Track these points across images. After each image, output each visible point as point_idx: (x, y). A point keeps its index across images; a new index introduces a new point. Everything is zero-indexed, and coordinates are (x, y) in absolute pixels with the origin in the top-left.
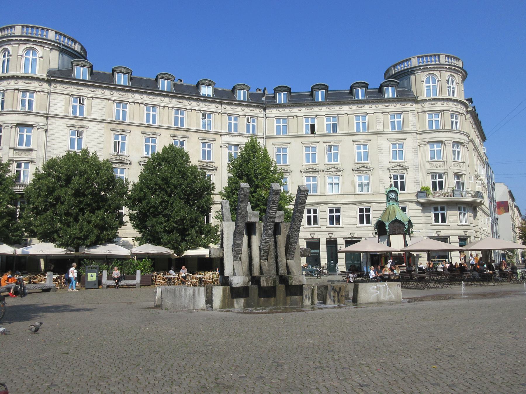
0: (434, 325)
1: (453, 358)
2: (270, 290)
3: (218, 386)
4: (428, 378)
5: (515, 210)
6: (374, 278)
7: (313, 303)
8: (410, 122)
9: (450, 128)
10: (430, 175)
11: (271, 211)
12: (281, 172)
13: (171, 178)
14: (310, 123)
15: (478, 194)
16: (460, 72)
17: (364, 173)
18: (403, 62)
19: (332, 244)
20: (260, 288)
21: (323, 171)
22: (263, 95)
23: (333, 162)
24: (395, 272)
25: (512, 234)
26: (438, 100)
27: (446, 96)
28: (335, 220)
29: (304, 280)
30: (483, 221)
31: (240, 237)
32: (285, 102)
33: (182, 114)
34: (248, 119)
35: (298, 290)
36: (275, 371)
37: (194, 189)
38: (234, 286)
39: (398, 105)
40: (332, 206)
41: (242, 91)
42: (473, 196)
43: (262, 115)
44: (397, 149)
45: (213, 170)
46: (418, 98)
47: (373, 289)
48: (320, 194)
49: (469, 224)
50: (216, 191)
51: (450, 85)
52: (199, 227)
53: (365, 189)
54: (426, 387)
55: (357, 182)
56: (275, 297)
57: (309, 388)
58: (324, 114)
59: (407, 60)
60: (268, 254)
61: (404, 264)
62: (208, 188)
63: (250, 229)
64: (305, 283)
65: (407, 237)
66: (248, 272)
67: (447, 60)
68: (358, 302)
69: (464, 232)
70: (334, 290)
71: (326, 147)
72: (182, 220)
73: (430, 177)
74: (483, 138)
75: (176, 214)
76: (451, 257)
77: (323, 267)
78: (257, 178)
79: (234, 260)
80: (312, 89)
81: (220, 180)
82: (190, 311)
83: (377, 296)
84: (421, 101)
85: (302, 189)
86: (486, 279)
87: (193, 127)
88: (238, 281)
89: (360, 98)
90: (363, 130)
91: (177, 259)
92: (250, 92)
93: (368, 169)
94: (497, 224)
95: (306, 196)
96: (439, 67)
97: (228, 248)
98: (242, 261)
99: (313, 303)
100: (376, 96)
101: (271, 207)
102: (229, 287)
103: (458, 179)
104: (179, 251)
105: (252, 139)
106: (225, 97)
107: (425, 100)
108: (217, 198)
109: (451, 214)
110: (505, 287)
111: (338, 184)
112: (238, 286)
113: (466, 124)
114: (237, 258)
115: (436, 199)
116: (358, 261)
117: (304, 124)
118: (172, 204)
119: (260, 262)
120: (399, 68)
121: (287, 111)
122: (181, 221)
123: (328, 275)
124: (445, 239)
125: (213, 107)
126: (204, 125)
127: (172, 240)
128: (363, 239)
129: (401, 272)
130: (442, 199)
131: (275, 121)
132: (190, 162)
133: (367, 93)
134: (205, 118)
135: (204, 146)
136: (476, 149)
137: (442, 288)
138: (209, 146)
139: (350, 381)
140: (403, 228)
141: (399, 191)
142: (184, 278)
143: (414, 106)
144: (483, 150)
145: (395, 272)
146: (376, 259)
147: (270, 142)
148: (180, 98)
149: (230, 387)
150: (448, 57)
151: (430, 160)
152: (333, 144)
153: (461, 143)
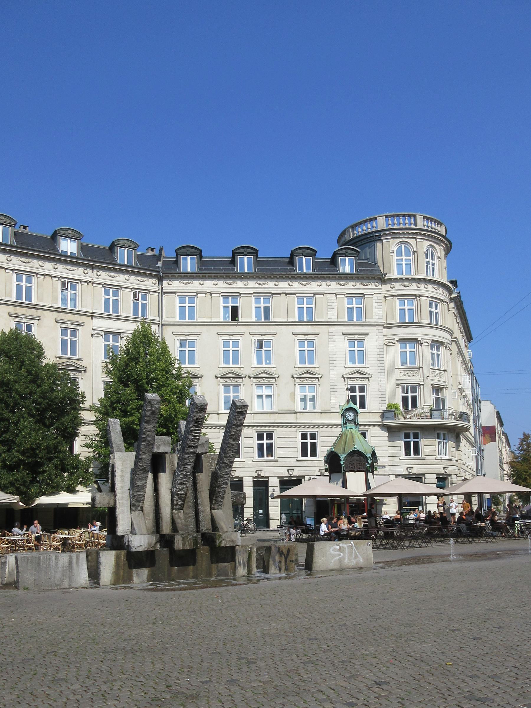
0: (434, 598)
1: (480, 641)
2: (187, 555)
3: (177, 697)
4: (460, 669)
5: (503, 438)
6: (326, 534)
7: (249, 573)
8: (374, 310)
9: (428, 321)
10: (400, 387)
11: (191, 437)
12: (188, 377)
13: (16, 382)
14: (230, 305)
15: (462, 416)
16: (442, 241)
17: (309, 382)
18: (366, 221)
19: (261, 485)
20: (173, 552)
21: (249, 377)
22: (159, 258)
23: (264, 365)
24: (357, 525)
25: (499, 472)
26: (413, 279)
27: (422, 275)
28: (266, 450)
29: (238, 538)
30: (467, 453)
31: (143, 475)
32: (193, 271)
33: (29, 281)
34: (135, 295)
35: (229, 554)
36: (248, 670)
37: (52, 401)
38: (134, 550)
39: (358, 284)
40: (261, 430)
41: (126, 251)
42: (455, 419)
43: (156, 289)
44: (356, 349)
45: (80, 371)
46: (385, 275)
47: (335, 550)
48: (319, 411)
49: (451, 458)
50: (87, 404)
51: (430, 260)
52: (62, 460)
53: (309, 404)
54: (463, 681)
55: (299, 394)
56: (194, 565)
57: (309, 690)
58: (252, 292)
59: (371, 220)
60: (184, 501)
61: (365, 514)
62: (74, 400)
63: (157, 463)
64: (239, 544)
65: (370, 475)
66: (153, 529)
67: (426, 223)
68: (313, 569)
69: (444, 468)
70: (281, 553)
71: (253, 341)
72: (33, 450)
73: (400, 389)
74: (469, 338)
75: (24, 439)
76: (426, 504)
77: (248, 519)
78: (151, 385)
79: (132, 510)
80: (235, 253)
81: (93, 386)
82: (65, 591)
83: (340, 560)
84: (390, 280)
85: (238, 404)
86: (475, 533)
87: (47, 302)
88: (140, 542)
89: (305, 271)
90: (308, 318)
91: (23, 511)
92: (138, 252)
93: (315, 376)
94: (482, 457)
95: (244, 414)
96: (416, 233)
97: (123, 493)
98: (145, 512)
99: (249, 573)
100: (327, 269)
101: (192, 431)
102: (125, 551)
103: (437, 394)
104: (27, 498)
105: (143, 325)
106: (97, 257)
107: (396, 280)
108: (87, 415)
109: (427, 443)
110: (501, 544)
111: (270, 397)
112: (140, 549)
113: (448, 317)
114: (137, 508)
115: (408, 422)
116: (297, 510)
117: (222, 305)
118: (16, 424)
119: (172, 513)
120: (360, 230)
121: (195, 285)
122: (32, 451)
123: (255, 531)
124: (419, 478)
125: (79, 273)
126: (64, 300)
127: (16, 480)
128: (307, 478)
129: (364, 525)
130: (415, 421)
131: (177, 298)
132: (44, 357)
133: (315, 264)
134: (67, 289)
135: (64, 333)
136: (460, 353)
137: (421, 547)
138: (74, 334)
139: (360, 678)
140: (364, 462)
141: (359, 410)
142: (38, 539)
143: (380, 287)
144: (468, 354)
145: (357, 525)
146: (323, 507)
147: (168, 331)
148: (24, 255)
149: (195, 697)
150: (428, 219)
151: (400, 366)
152: (264, 337)
153: (442, 343)
